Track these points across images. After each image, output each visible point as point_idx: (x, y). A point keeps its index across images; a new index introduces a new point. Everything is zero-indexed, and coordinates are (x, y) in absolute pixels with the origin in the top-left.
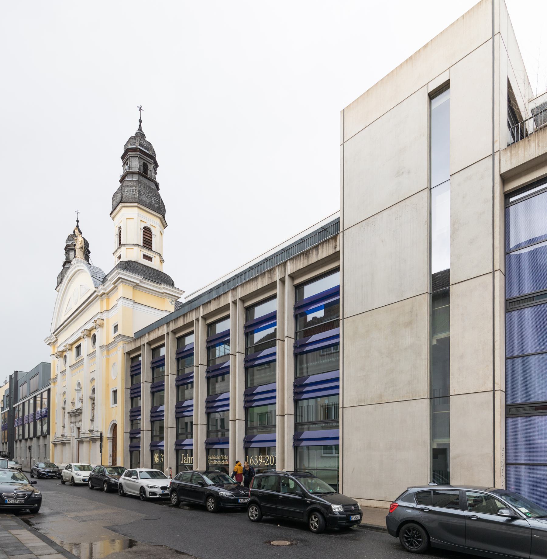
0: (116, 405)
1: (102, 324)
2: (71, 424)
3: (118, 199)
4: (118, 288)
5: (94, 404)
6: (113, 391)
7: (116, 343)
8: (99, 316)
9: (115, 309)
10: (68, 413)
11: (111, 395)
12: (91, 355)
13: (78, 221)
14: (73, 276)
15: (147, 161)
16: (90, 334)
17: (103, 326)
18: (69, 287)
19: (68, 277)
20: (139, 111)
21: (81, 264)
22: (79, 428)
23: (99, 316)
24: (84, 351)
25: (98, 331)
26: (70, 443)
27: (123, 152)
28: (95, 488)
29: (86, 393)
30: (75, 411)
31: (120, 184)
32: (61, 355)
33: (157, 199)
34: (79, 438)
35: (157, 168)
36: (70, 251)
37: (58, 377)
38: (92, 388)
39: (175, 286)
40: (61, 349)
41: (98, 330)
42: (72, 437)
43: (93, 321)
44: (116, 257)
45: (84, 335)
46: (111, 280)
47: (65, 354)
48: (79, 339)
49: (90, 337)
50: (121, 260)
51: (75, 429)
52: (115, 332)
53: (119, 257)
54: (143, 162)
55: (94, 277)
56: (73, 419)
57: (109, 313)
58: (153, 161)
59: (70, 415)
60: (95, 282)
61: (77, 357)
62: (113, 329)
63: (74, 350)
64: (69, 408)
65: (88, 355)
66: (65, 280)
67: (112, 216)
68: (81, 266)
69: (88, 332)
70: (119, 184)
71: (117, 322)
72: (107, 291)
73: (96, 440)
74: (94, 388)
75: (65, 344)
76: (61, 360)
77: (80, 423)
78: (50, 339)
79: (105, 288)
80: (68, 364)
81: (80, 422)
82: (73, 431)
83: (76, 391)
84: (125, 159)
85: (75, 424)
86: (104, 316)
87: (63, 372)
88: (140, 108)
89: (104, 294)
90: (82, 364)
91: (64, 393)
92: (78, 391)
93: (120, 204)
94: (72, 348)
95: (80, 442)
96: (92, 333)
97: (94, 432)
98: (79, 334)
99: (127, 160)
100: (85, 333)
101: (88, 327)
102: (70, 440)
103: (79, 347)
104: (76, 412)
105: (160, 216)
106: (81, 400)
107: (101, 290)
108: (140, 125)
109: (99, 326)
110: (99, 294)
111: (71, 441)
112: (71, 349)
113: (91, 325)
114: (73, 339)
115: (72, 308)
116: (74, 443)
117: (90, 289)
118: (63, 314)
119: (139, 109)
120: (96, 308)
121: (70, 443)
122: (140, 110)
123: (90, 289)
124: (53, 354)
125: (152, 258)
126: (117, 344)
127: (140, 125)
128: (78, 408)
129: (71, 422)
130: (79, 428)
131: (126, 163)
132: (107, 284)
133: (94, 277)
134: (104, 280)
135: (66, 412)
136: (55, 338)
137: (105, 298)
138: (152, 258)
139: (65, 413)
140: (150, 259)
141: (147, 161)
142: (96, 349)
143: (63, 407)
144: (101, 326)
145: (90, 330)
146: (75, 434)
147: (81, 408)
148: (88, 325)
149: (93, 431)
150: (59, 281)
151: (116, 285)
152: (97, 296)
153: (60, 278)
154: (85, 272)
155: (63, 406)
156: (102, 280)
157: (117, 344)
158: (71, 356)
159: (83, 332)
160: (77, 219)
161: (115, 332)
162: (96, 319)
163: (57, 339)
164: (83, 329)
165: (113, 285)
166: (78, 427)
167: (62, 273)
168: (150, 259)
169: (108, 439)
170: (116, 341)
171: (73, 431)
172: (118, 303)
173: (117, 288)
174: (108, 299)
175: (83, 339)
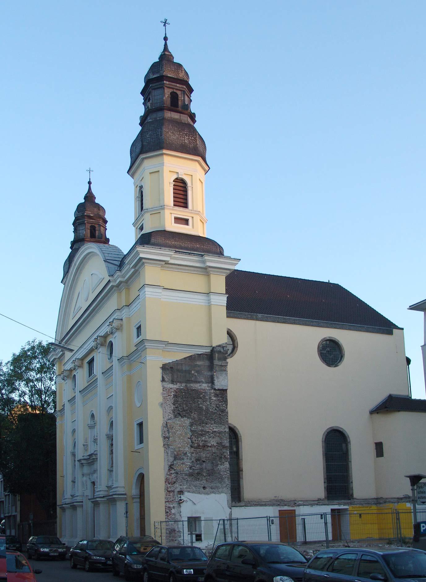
0: (142, 445)
1: (120, 325)
2: (83, 477)
3: (138, 150)
4: (140, 272)
5: (112, 445)
6: (137, 424)
7: (140, 352)
8: (115, 316)
9: (138, 302)
10: (79, 461)
11: (136, 429)
12: (107, 372)
13: (90, 183)
14: (82, 262)
15: (176, 89)
16: (105, 341)
17: (122, 329)
18: (78, 278)
19: (75, 265)
20: (164, 26)
21: (91, 246)
22: (93, 483)
23: (115, 316)
24: (98, 368)
25: (78, 373)
26: (82, 506)
27: (143, 85)
28: (78, 566)
29: (102, 428)
30: (88, 457)
31: (140, 128)
32: (68, 375)
33: (192, 137)
34: (94, 498)
35: (191, 94)
36: (80, 225)
37: (65, 408)
38: (110, 421)
39: (226, 254)
40: (69, 366)
41: (115, 336)
42: (85, 496)
43: (108, 323)
44: (137, 228)
45: (97, 345)
46: (129, 263)
47: (74, 373)
48: (91, 351)
49: (105, 346)
50: (143, 232)
51: (89, 484)
52: (138, 337)
53: (142, 228)
54: (170, 92)
55: (108, 262)
56: (86, 470)
57: (129, 309)
58: (185, 87)
59: (82, 464)
60: (108, 268)
61: (138, 338)
62: (135, 331)
63: (86, 366)
64: (81, 454)
65: (103, 373)
66: (73, 270)
67: (131, 172)
68: (91, 248)
69: (102, 339)
70: (140, 128)
71: (140, 321)
72: (58, 356)
73: (115, 500)
74: (112, 421)
75: (74, 359)
76: (69, 382)
77: (95, 475)
78: (54, 353)
79: (123, 274)
80: (115, 359)
81: (94, 473)
82: (87, 488)
83: (89, 427)
84: (147, 93)
85: (88, 476)
86: (124, 314)
87: (72, 400)
88: (165, 23)
89: (121, 282)
90: (96, 387)
91: (111, 408)
92: (92, 427)
93: (141, 155)
94: (82, 364)
95: (96, 504)
96: (108, 340)
97: (113, 488)
98: (91, 344)
99: (149, 94)
100: (98, 341)
101: (102, 332)
102: (82, 502)
103: (91, 362)
104: (89, 458)
105: (199, 159)
106: (95, 441)
107: (119, 277)
108: (166, 45)
109: (117, 329)
110: (115, 285)
111: (84, 504)
112: (81, 366)
113: (105, 329)
114: (81, 354)
115: (81, 307)
116: (89, 505)
117: (104, 278)
118: (71, 317)
119: (164, 24)
120: (112, 304)
121: (83, 507)
122: (164, 25)
123: (104, 278)
124: (59, 375)
125: (189, 219)
126: (141, 353)
127: (166, 45)
128: (92, 452)
129: (83, 475)
130: (93, 483)
131: (147, 100)
132: (125, 268)
133: (108, 262)
134: (121, 265)
135: (76, 460)
136: (61, 351)
137: (124, 287)
138: (189, 219)
139: (75, 461)
140: (186, 222)
141: (176, 89)
142: (114, 363)
143: (73, 452)
144: (119, 329)
145: (105, 337)
146: (89, 493)
147: (95, 453)
148: (100, 331)
149: (75, 496)
150: (66, 270)
151: (137, 268)
152: (112, 287)
153: (67, 266)
154: (98, 255)
155: (73, 451)
156: (118, 263)
157: (141, 353)
158: (82, 375)
159: (96, 339)
160: (89, 181)
161: (138, 337)
162: (111, 320)
163: (64, 352)
164: (95, 336)
165: (133, 270)
166: (93, 481)
167: (142, 137)
168: (186, 222)
169: (133, 498)
170: (139, 349)
171: (85, 487)
172: (141, 294)
173: (138, 272)
174: (128, 288)
175: (96, 350)
